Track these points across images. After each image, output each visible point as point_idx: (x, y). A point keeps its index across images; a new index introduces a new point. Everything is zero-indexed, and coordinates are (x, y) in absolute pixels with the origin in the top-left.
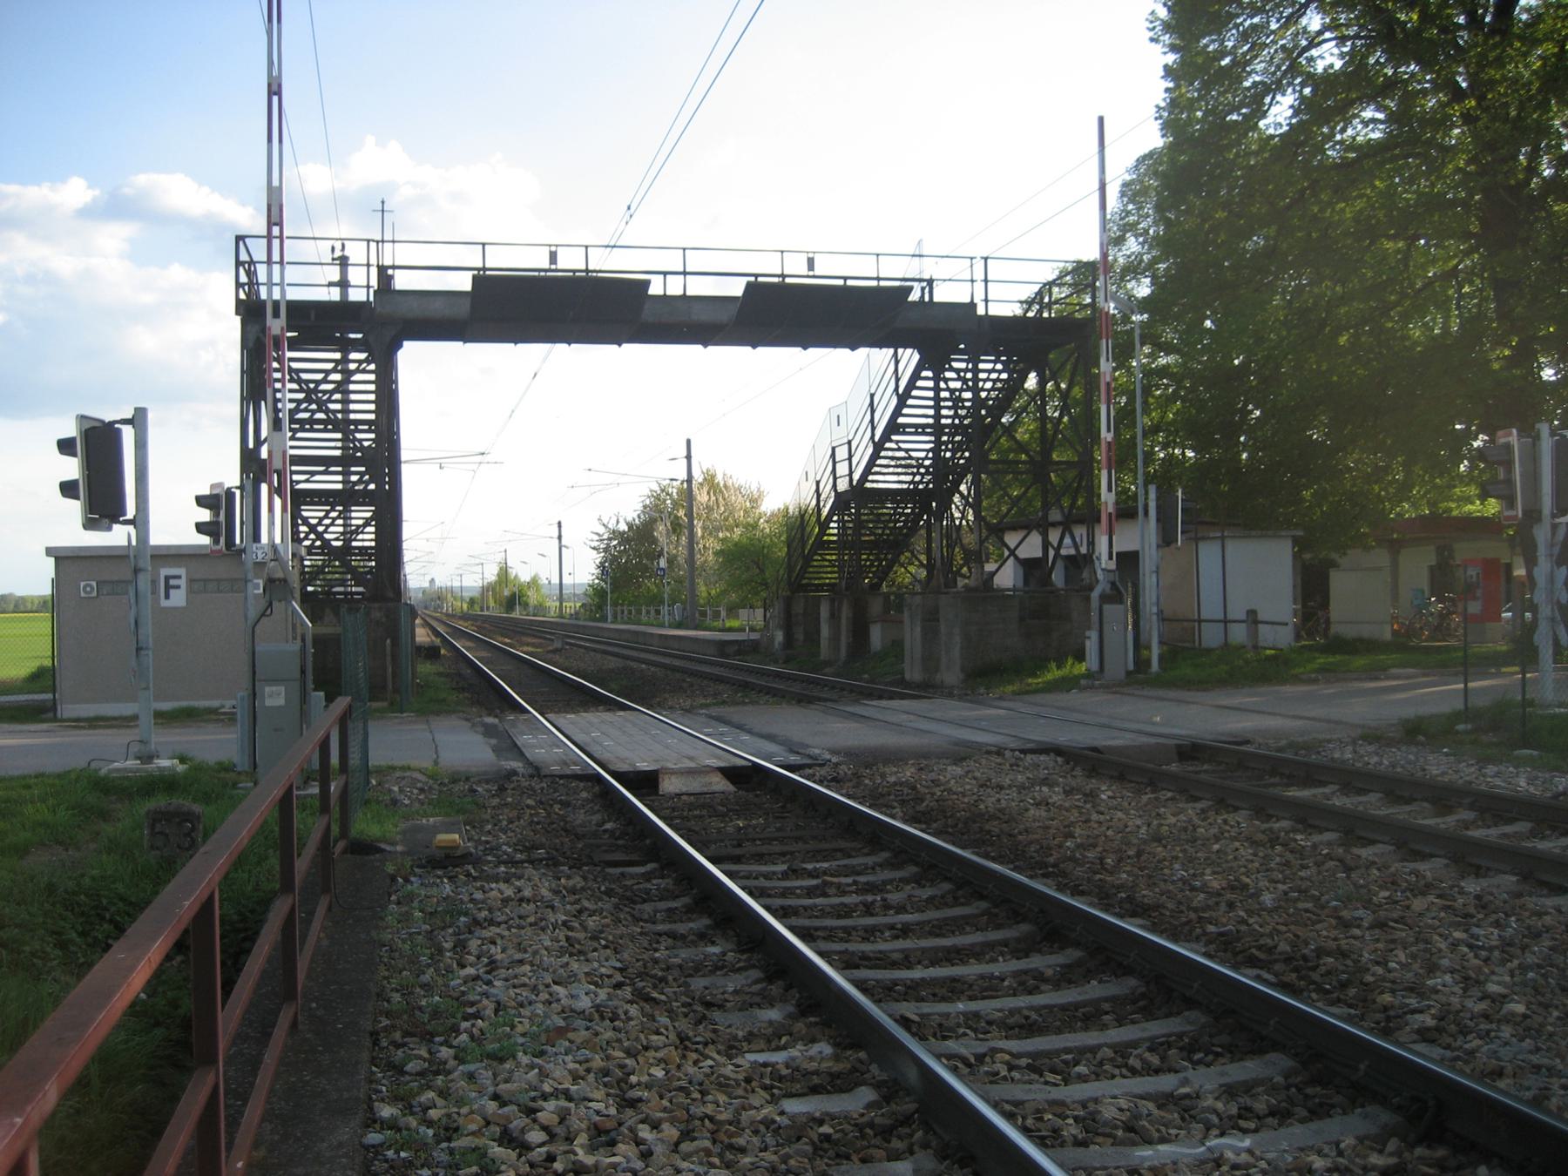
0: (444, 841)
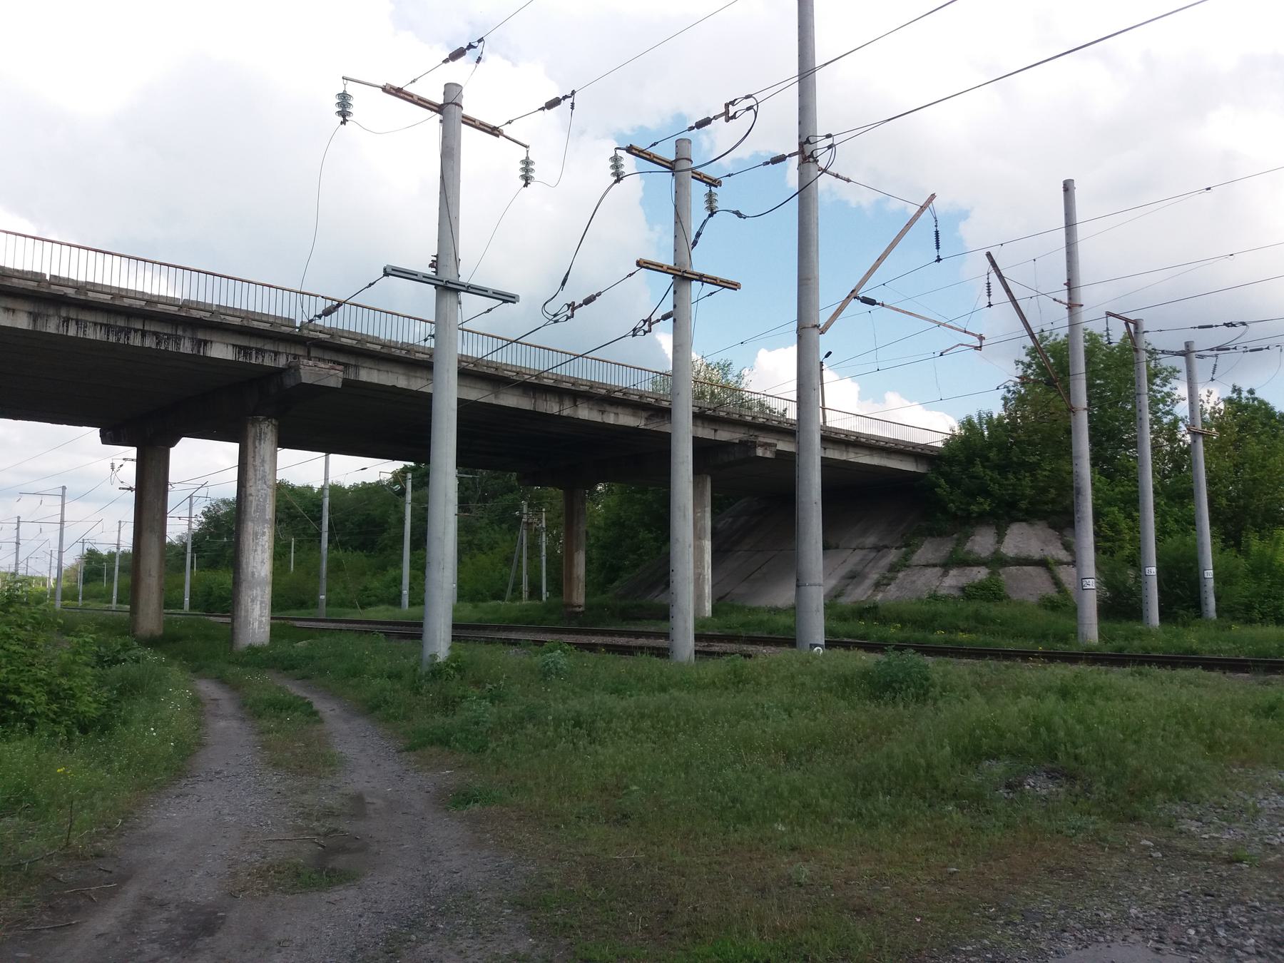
0: (54, 290)
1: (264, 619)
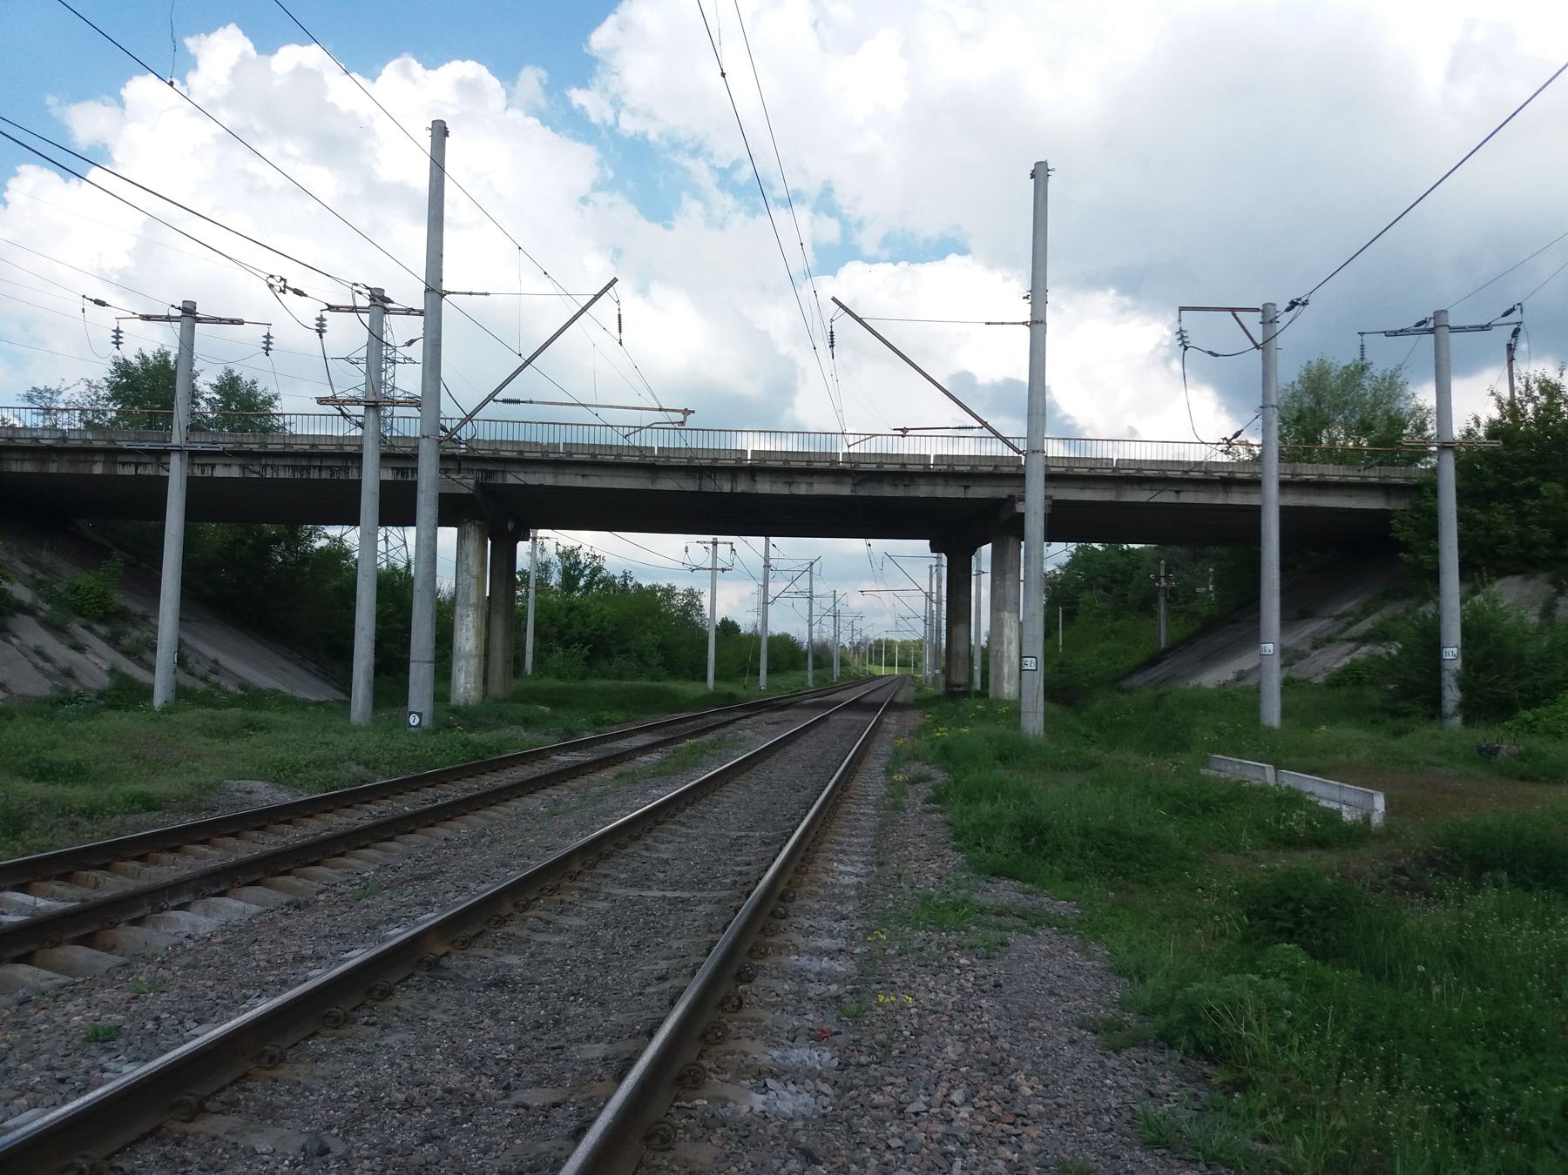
1: (468, 686)
